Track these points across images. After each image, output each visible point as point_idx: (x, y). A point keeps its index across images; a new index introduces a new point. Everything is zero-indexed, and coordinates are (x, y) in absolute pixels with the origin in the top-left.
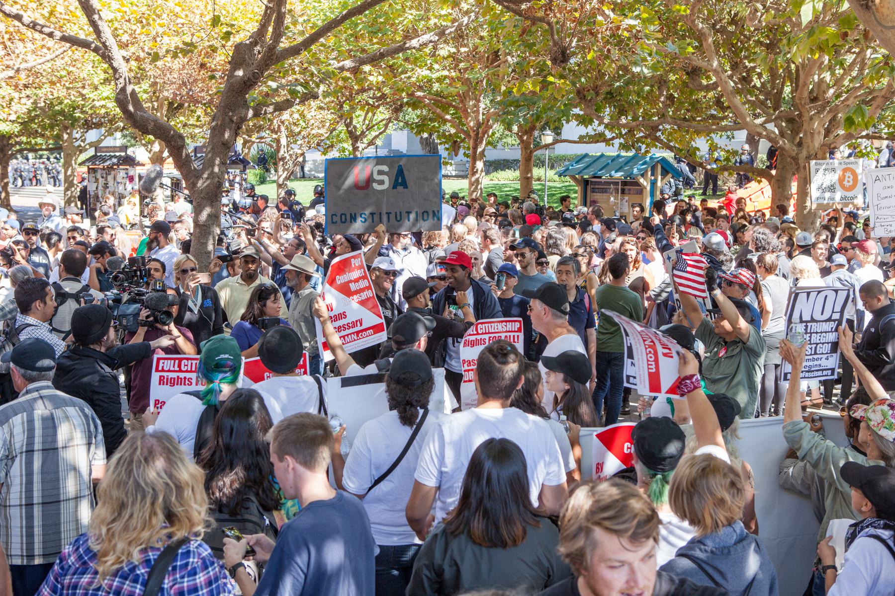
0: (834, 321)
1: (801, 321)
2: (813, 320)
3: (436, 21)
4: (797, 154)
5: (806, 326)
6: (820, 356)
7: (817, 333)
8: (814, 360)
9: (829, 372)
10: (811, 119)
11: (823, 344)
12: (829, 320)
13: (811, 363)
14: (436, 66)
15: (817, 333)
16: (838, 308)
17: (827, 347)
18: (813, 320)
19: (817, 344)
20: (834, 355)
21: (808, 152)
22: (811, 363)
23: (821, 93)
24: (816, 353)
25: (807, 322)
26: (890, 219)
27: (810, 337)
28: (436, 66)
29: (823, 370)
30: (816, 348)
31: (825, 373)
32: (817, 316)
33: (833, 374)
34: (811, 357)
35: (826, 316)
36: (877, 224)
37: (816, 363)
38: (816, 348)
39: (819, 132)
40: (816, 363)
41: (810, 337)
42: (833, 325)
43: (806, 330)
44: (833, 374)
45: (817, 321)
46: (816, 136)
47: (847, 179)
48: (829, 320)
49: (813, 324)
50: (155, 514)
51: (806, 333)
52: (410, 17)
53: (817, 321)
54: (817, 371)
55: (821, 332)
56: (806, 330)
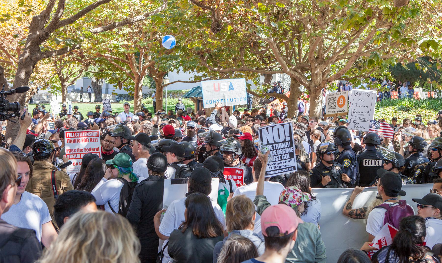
0: (288, 141)
1: (268, 144)
2: (275, 143)
3: (121, 15)
4: (309, 85)
5: (273, 147)
6: (284, 161)
7: (279, 149)
8: (281, 163)
9: (293, 168)
10: (316, 68)
11: (285, 154)
12: (285, 141)
13: (280, 165)
14: (120, 39)
15: (279, 149)
16: (288, 134)
17: (287, 156)
18: (275, 143)
19: (281, 155)
20: (293, 159)
21: (315, 84)
22: (280, 165)
23: (320, 55)
24: (282, 160)
25: (272, 144)
26: (359, 120)
27: (276, 151)
28: (120, 39)
29: (288, 168)
30: (281, 157)
31: (290, 169)
32: (277, 140)
33: (295, 169)
34: (279, 162)
35: (282, 139)
36: (352, 121)
37: (283, 164)
38: (281, 157)
39: (320, 74)
40: (283, 164)
41: (276, 151)
42: (288, 144)
43: (273, 148)
44: (295, 169)
45: (278, 143)
46: (318, 76)
47: (341, 101)
48: (285, 141)
49: (276, 145)
50: (81, 255)
51: (274, 150)
52: (106, 13)
53: (278, 143)
54: (284, 168)
55: (282, 149)
56: (273, 148)
